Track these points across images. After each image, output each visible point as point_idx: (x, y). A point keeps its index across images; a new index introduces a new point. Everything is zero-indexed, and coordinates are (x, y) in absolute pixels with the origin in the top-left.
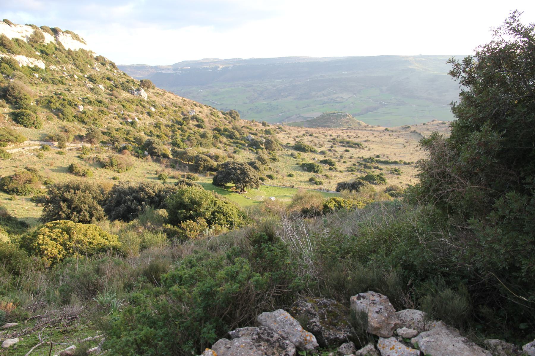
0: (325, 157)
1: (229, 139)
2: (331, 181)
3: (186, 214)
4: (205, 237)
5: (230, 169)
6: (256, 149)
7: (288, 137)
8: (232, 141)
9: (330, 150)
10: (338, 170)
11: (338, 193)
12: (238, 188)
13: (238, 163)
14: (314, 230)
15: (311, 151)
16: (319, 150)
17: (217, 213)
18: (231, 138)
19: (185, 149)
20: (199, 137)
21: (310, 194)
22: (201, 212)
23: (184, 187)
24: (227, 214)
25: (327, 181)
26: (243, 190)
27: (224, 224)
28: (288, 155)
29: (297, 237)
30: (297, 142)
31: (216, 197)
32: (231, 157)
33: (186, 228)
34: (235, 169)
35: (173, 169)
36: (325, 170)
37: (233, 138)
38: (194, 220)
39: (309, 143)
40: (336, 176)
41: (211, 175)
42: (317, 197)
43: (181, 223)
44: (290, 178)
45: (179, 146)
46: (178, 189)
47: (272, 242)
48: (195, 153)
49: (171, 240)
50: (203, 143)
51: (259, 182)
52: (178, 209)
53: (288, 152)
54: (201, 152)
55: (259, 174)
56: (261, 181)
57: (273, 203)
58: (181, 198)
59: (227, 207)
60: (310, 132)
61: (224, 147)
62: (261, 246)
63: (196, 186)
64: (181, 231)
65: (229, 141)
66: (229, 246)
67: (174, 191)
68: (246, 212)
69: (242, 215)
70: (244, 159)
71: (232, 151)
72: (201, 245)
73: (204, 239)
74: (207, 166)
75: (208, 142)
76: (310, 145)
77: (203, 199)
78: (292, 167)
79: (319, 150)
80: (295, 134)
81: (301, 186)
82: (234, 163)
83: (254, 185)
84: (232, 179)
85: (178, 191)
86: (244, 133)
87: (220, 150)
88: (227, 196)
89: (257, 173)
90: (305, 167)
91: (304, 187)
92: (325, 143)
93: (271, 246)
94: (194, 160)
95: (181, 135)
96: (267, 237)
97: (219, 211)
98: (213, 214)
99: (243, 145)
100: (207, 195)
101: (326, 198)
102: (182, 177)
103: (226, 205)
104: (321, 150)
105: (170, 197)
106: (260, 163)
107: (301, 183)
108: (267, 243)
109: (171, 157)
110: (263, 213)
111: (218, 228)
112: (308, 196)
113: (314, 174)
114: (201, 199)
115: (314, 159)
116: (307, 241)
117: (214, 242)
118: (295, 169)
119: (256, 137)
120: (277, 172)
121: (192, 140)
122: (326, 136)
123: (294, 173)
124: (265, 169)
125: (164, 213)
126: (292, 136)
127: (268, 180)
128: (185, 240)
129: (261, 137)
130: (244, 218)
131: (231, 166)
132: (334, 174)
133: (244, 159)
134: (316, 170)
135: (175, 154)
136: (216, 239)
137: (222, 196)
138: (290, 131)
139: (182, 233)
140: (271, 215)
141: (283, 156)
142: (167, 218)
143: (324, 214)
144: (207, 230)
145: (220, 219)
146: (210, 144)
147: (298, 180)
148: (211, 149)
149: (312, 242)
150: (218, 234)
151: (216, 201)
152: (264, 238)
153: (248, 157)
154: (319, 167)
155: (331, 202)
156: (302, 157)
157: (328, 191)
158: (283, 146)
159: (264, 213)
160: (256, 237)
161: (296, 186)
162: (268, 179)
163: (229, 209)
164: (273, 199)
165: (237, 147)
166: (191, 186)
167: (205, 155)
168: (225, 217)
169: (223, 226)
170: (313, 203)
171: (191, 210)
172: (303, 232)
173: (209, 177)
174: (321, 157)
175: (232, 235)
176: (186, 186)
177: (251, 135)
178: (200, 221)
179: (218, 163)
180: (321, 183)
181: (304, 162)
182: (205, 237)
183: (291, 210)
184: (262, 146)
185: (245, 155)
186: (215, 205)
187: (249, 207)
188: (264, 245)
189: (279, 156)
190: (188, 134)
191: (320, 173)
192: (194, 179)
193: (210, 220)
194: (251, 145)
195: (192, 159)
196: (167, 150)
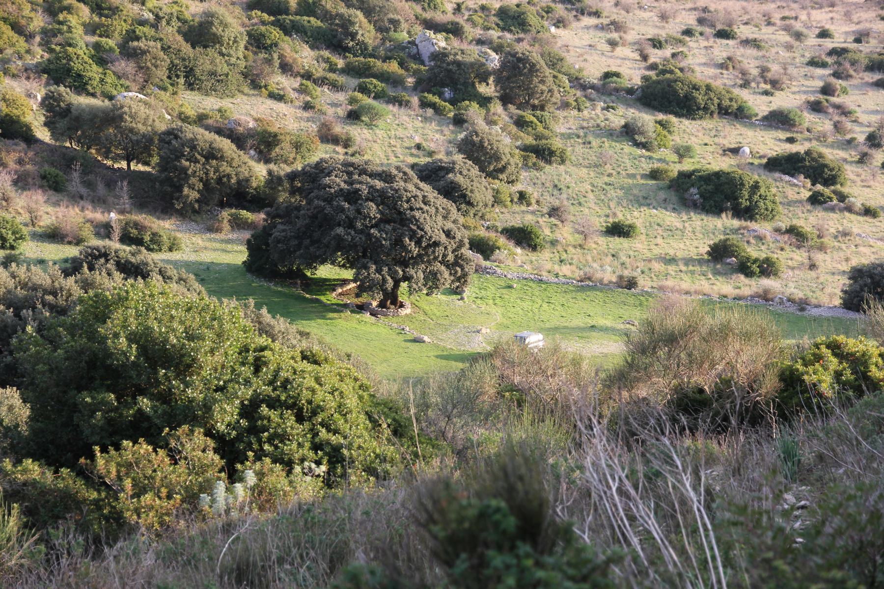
0: (791, 140)
1: (326, 53)
2: (819, 257)
3: (116, 409)
4: (211, 523)
5: (329, 199)
6: (453, 102)
7: (613, 44)
8: (340, 63)
9: (816, 107)
10: (858, 203)
11: (852, 315)
12: (370, 289)
13: (370, 168)
14: (737, 491)
15: (724, 112)
16: (760, 105)
17: (271, 406)
18: (338, 47)
19: (111, 98)
20: (180, 38)
21: (711, 321)
22: (191, 401)
23: (107, 283)
24: (314, 413)
25: (800, 256)
26: (391, 300)
27: (302, 460)
28: (611, 134)
29: (656, 531)
30: (653, 67)
31: (264, 330)
32: (335, 140)
33: (119, 478)
34: (353, 196)
35: (55, 197)
36: (790, 203)
37: (346, 49)
38: (156, 442)
39: (712, 71)
40: (845, 234)
41: (238, 224)
42: (747, 336)
43: (92, 457)
44: (617, 242)
45: (81, 85)
46: (77, 292)
47: (535, 544)
48: (161, 117)
49: (45, 540)
50: (198, 72)
51: (467, 261)
52: (80, 389)
53: (610, 115)
54: (191, 113)
55: (471, 221)
56: (478, 258)
57: (535, 360)
58: (92, 336)
59: (318, 380)
60: (721, 15)
61: (302, 90)
62: (482, 563)
63: (166, 278)
64: (94, 495)
65: (327, 61)
66: (324, 566)
67: (61, 302)
68: (406, 402)
69: (387, 416)
70: (399, 150)
71: (341, 112)
72: (192, 562)
73: (202, 533)
74: (219, 180)
75: (222, 67)
76: (717, 84)
77: (201, 338)
78: (627, 190)
79: (760, 105)
80: (643, 29)
81: (670, 283)
82: (349, 168)
83: (446, 274)
84: (340, 245)
85: (81, 301)
86: (395, 23)
87: (280, 107)
88: (316, 328)
89: (462, 220)
90: (693, 190)
91: (685, 286)
92: (791, 70)
93: (529, 563)
94: (155, 150)
95: (91, 29)
96: (511, 522)
97: (278, 399)
98: (249, 410)
99: (394, 81)
100: (220, 319)
101: (793, 342)
102: (98, 235)
103: (309, 367)
104: (774, 107)
105: (39, 330)
106: (475, 171)
107: (672, 269)
108: (513, 548)
109: (43, 135)
110: (486, 407)
111: (271, 479)
112: (704, 331)
113: (736, 223)
114: (191, 338)
115: (735, 151)
116: (700, 548)
117: (255, 548)
118: (643, 201)
119: (456, 43)
120: (554, 212)
121: (144, 52)
122: (798, 36)
123: (637, 217)
124: (497, 200)
125: (11, 408)
126: (631, 36)
127: (512, 254)
128: (112, 539)
129: (480, 42)
130: (399, 431)
131: (338, 181)
132: (833, 222)
133: (399, 150)
134: (745, 203)
135: (62, 124)
136: (261, 532)
137: (293, 328)
138: (618, 15)
139: (96, 502)
140: (527, 418)
141: (584, 134)
142: (24, 429)
143: (785, 417)
144: (221, 488)
145: (284, 437)
146: (235, 78)
147: (657, 251)
148: (240, 99)
149: (726, 548)
150: (273, 507)
151: (263, 349)
152: (497, 524)
153: (417, 139)
154: (762, 191)
155: (818, 358)
156: (677, 139)
157: (802, 305)
158: (584, 87)
159: (494, 407)
160: (461, 520)
161: (644, 283)
162: (511, 245)
163: (328, 387)
164: (535, 340)
165: (363, 89)
166: (145, 276)
167: (208, 128)
168: (307, 425)
169: (297, 469)
170: (731, 366)
171: (143, 392)
172: (684, 502)
173: (227, 233)
174: (771, 143)
175: (342, 514)
176: (118, 276)
177: (430, 33)
178: (188, 446)
179: (272, 166)
180: (767, 268)
181: (687, 165)
182: (211, 523)
183: (625, 394)
184: (482, 89)
185: (401, 132)
186: (257, 370)
187: (418, 381)
188: (497, 560)
189: (567, 137)
190: (126, 27)
191: (765, 218)
192: (155, 244)
193: (233, 442)
194: (426, 84)
195: (147, 150)
196: (23, 100)
